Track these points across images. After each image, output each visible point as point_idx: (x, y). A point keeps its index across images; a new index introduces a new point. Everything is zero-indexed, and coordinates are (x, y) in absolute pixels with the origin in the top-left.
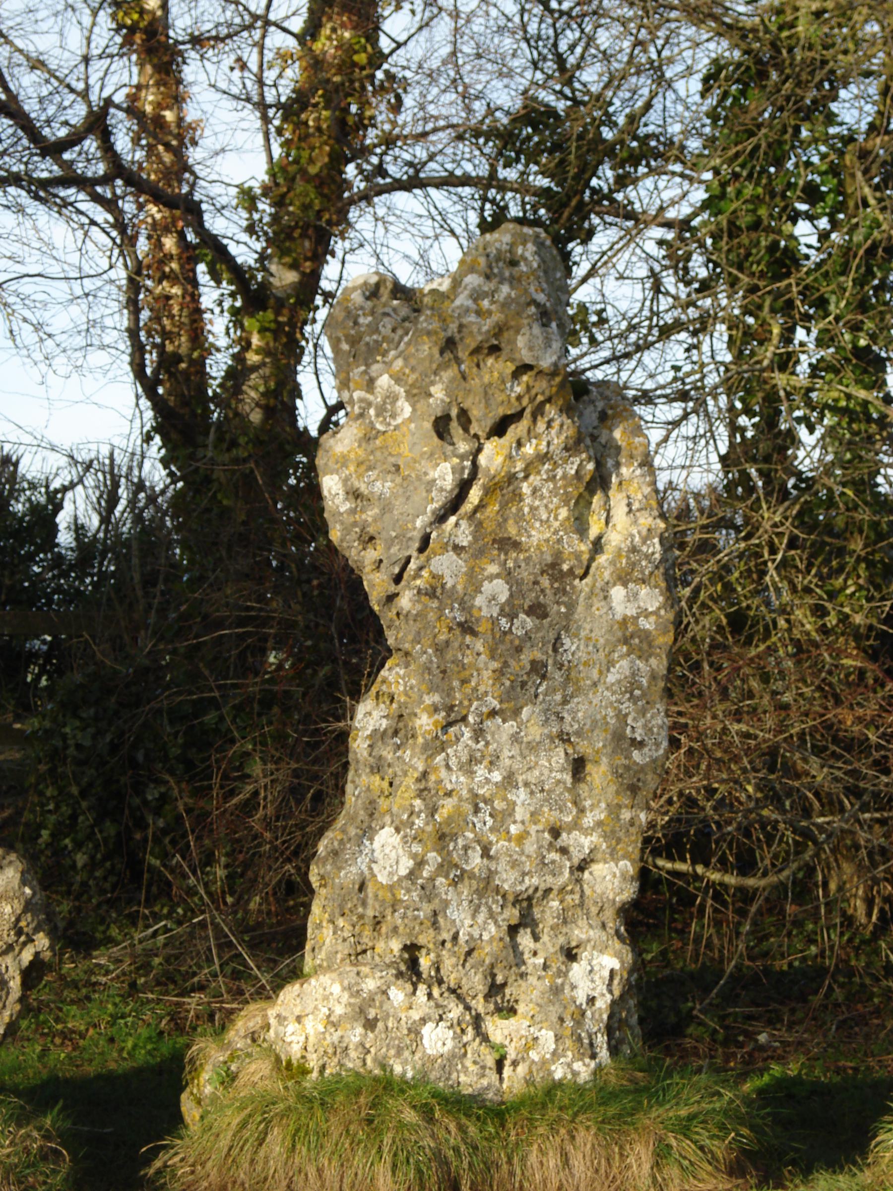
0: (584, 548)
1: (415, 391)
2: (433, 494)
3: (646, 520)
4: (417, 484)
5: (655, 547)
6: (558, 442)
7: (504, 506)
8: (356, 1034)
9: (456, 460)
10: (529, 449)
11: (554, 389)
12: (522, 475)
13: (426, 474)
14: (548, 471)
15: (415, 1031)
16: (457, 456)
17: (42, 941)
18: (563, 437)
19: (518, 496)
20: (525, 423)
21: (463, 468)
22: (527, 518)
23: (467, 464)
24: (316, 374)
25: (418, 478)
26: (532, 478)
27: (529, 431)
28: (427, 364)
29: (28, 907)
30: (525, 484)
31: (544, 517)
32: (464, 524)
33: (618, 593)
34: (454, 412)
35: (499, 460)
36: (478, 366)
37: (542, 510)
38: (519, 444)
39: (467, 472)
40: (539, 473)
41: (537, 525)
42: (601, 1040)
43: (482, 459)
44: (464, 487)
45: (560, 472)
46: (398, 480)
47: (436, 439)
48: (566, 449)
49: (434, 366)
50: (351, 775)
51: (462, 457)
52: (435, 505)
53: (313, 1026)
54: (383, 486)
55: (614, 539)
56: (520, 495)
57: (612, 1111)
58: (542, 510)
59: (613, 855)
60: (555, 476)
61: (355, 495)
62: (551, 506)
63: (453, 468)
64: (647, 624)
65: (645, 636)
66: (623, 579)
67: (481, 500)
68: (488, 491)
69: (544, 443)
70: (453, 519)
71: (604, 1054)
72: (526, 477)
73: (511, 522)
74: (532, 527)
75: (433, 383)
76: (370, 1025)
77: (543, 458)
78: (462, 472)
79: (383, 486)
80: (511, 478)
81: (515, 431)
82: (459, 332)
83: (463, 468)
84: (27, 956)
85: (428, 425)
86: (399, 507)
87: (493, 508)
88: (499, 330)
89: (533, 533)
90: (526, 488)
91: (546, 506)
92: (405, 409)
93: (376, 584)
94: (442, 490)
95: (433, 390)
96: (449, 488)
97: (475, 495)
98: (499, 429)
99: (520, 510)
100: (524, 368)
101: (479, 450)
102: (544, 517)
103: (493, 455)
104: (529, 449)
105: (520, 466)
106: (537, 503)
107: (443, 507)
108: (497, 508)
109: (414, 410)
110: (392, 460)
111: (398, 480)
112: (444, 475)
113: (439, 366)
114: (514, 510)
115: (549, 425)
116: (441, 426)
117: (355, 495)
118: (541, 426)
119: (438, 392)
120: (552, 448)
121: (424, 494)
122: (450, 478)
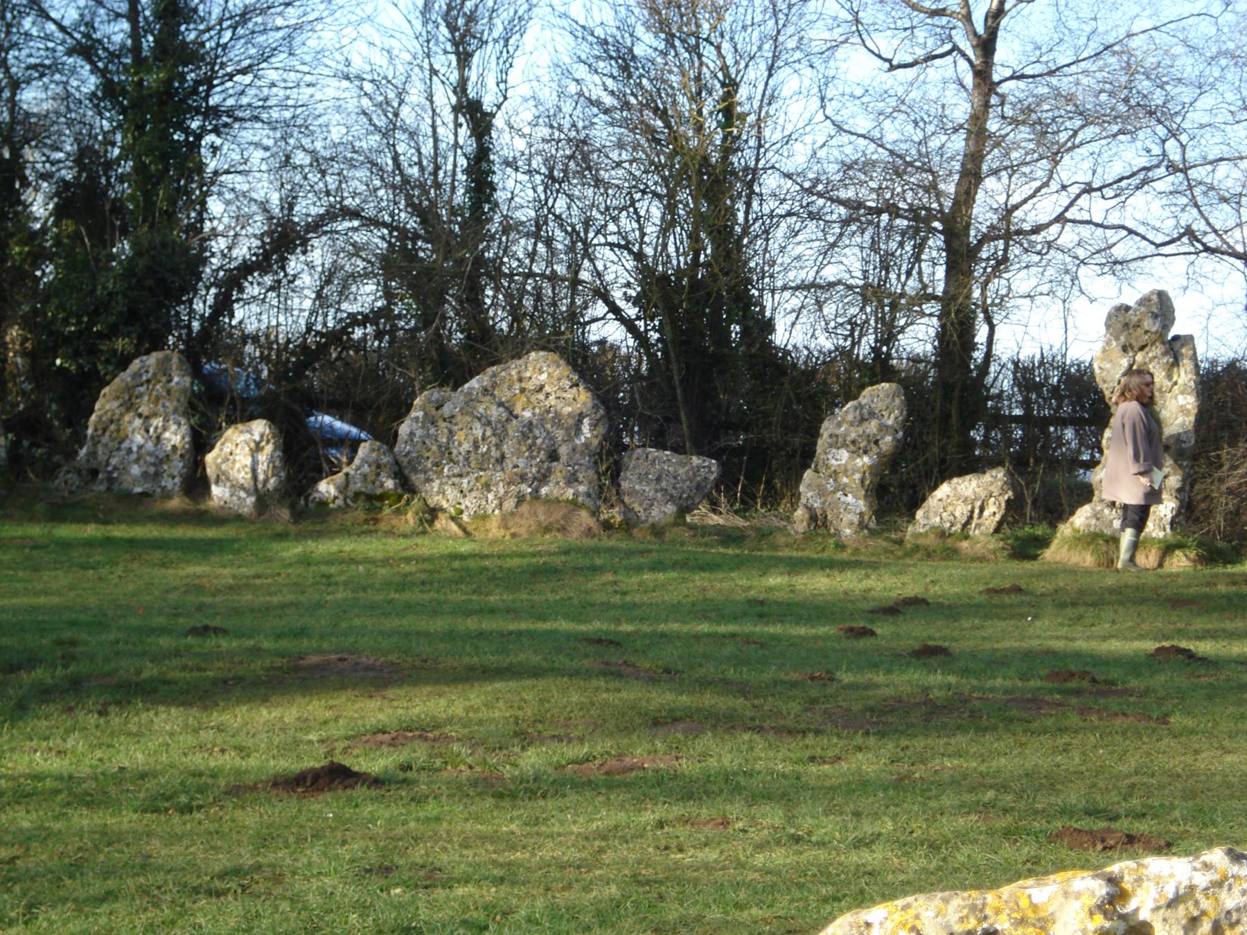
0: (1170, 384)
3: (1190, 376)
5: (1192, 384)
8: (1093, 522)
15: (1111, 522)
17: (1010, 493)
24: (1143, 258)
29: (1005, 483)
33: (1180, 397)
42: (1168, 527)
50: (529, 682)
53: (1083, 519)
54: (1108, 366)
55: (1180, 381)
59: (1175, 474)
61: (1100, 368)
64: (1189, 407)
65: (1188, 411)
66: (1182, 393)
71: (1168, 530)
76: (1098, 519)
77: (1155, 357)
79: (1108, 366)
81: (1147, 349)
84: (1006, 497)
86: (1112, 371)
88: (1139, 321)
92: (1114, 343)
93: (1107, 393)
98: (1142, 348)
100: (1146, 332)
117: (1100, 368)
119: (1122, 338)
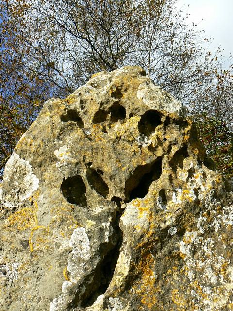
1: (40, 159)
2: (69, 267)
4: (48, 258)
6: (206, 189)
7: (162, 275)
9: (91, 223)
10: (176, 201)
11: (187, 137)
12: (175, 231)
13: (58, 245)
14: (203, 224)
16: (93, 218)
18: (209, 184)
19: (177, 259)
20: (163, 181)
21: (102, 230)
22: (194, 284)
23: (106, 224)
25: (50, 251)
26: (187, 234)
27: (171, 180)
28: (50, 130)
30: (181, 244)
31: (213, 280)
32: (115, 302)
34: (83, 174)
35: (145, 215)
36: (105, 131)
37: (209, 273)
38: (164, 199)
39: (107, 234)
40: (193, 227)
41: (208, 290)
43: (125, 220)
44: (107, 255)
45: (216, 223)
46: (27, 257)
47: (66, 203)
48: (215, 196)
49: (57, 131)
51: (99, 218)
52: (74, 281)
56: (179, 257)
57: (140, 263)
58: (209, 273)
60: (212, 230)
62: (218, 266)
63: (89, 232)
67: (132, 269)
68: (140, 257)
69: (192, 191)
70: (100, 299)
72: (181, 234)
73: (175, 292)
74: (203, 294)
75: (56, 147)
77: (195, 207)
78: (102, 236)
80: (164, 235)
82: (82, 107)
83: (102, 230)
85: (56, 191)
87: (149, 278)
89: (206, 302)
90: (183, 248)
91: (212, 267)
94: (79, 261)
95: (57, 153)
96: (87, 256)
97: (123, 264)
98: (137, 186)
99: (183, 276)
101: (120, 212)
102: (213, 280)
103: (136, 216)
104: (176, 201)
105: (170, 220)
106: (201, 264)
107: (84, 282)
108: (154, 276)
109: (42, 181)
110: (20, 237)
111: (27, 257)
112: (81, 242)
113: (61, 130)
114: (175, 276)
115: (191, 172)
116: (73, 190)
118: (183, 175)
120: (201, 197)
121: (57, 269)
122: (87, 244)
